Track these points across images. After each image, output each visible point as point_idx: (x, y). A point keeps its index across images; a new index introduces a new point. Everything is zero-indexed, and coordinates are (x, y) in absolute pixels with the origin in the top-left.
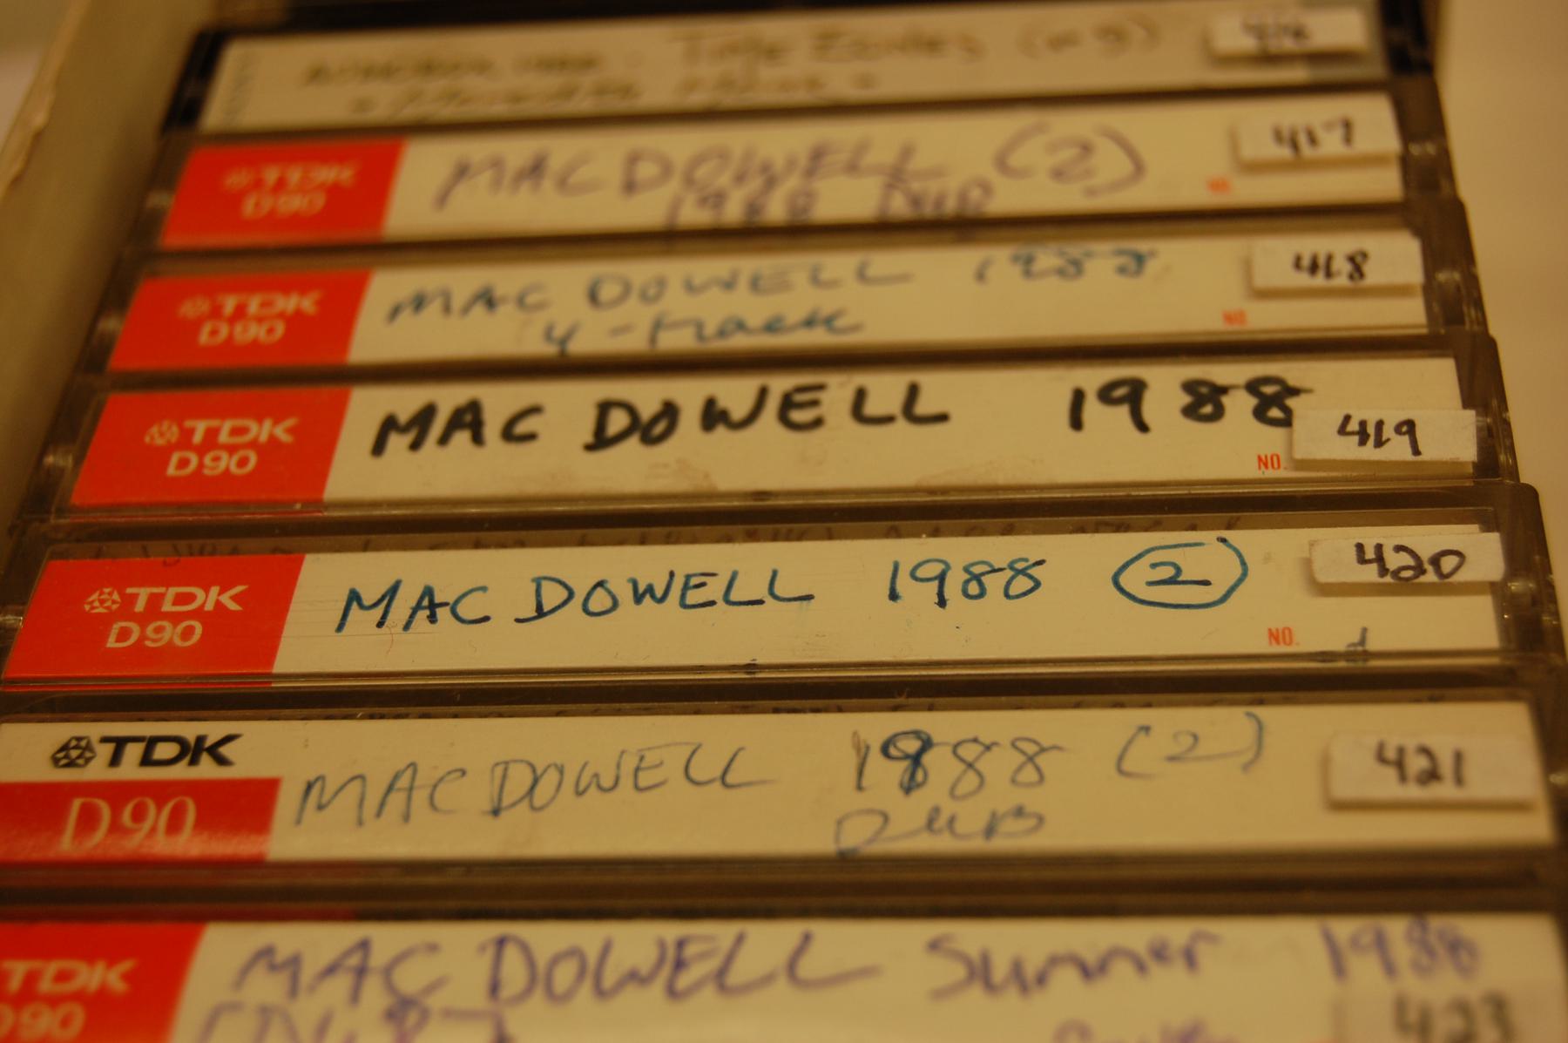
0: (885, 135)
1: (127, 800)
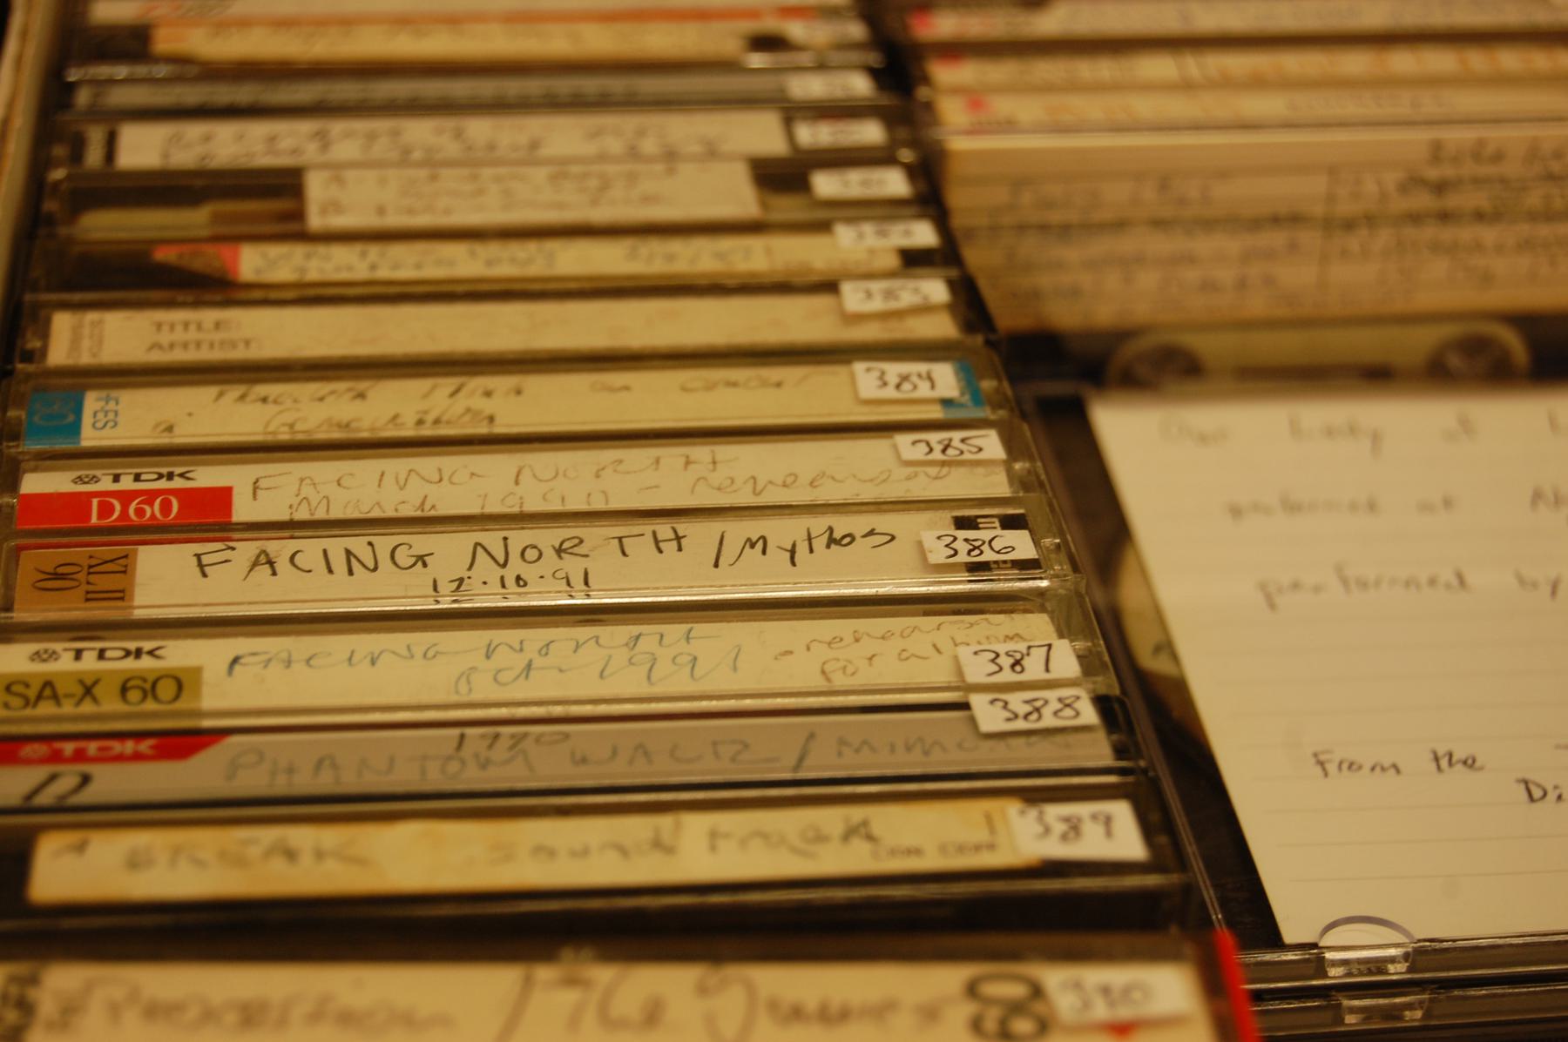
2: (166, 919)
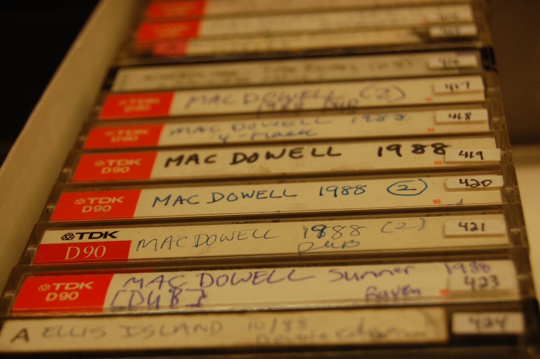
0: (325, 90)
1: (108, 212)
2: (123, 269)
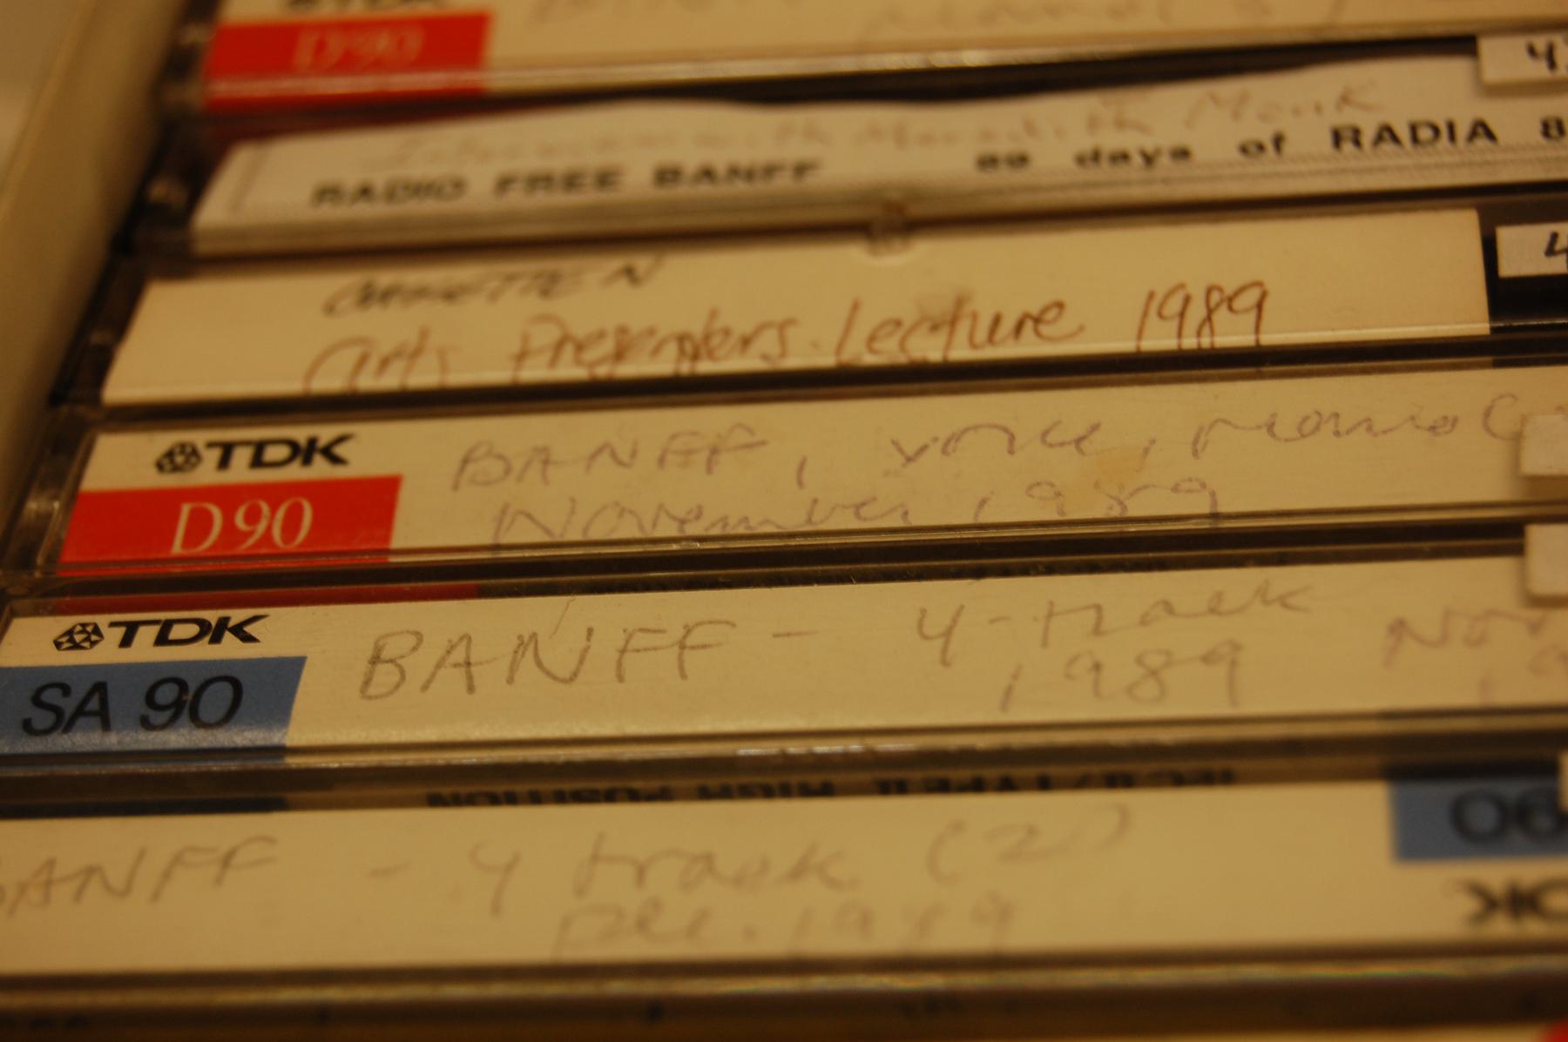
1: (241, 502)
